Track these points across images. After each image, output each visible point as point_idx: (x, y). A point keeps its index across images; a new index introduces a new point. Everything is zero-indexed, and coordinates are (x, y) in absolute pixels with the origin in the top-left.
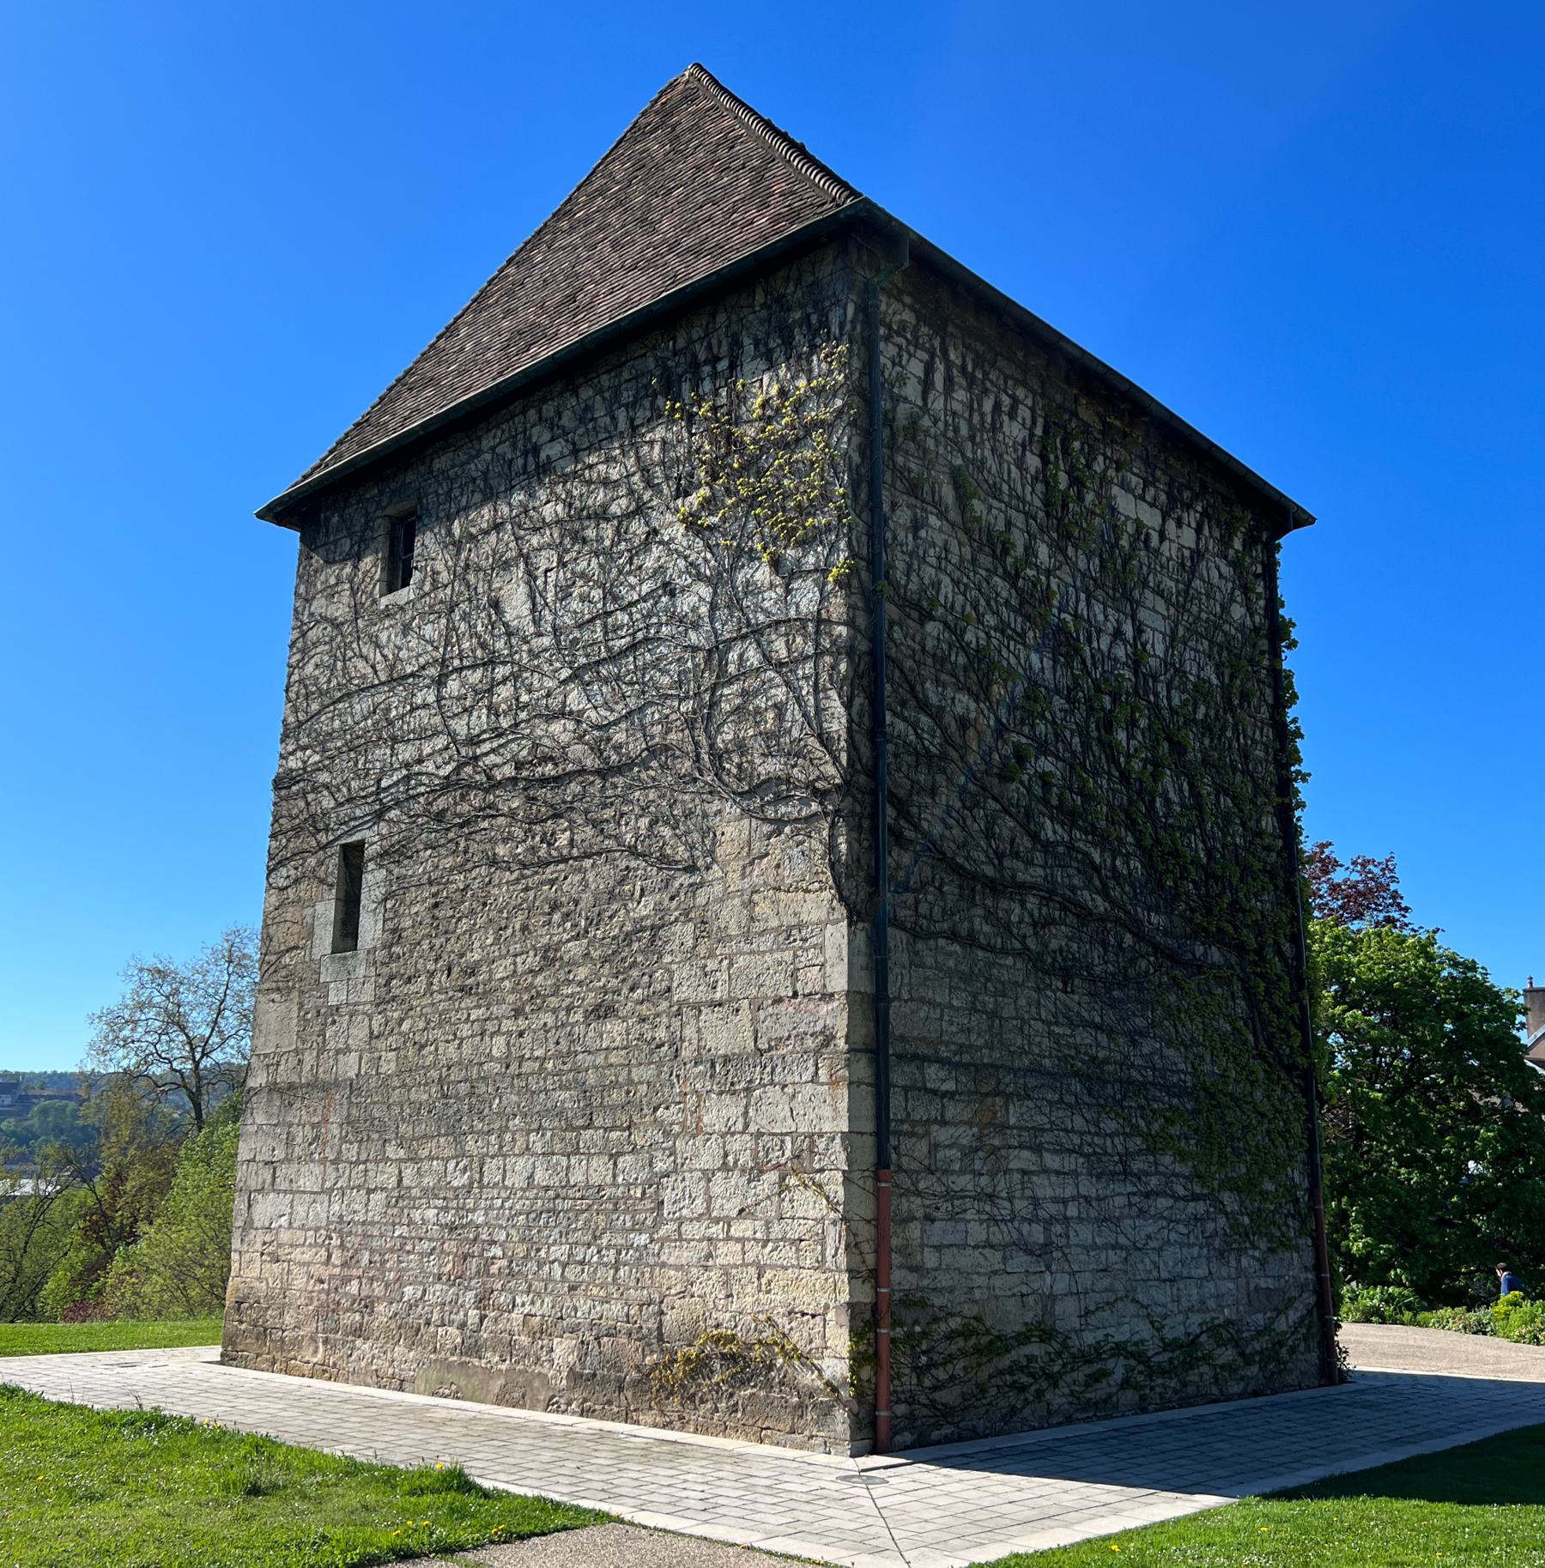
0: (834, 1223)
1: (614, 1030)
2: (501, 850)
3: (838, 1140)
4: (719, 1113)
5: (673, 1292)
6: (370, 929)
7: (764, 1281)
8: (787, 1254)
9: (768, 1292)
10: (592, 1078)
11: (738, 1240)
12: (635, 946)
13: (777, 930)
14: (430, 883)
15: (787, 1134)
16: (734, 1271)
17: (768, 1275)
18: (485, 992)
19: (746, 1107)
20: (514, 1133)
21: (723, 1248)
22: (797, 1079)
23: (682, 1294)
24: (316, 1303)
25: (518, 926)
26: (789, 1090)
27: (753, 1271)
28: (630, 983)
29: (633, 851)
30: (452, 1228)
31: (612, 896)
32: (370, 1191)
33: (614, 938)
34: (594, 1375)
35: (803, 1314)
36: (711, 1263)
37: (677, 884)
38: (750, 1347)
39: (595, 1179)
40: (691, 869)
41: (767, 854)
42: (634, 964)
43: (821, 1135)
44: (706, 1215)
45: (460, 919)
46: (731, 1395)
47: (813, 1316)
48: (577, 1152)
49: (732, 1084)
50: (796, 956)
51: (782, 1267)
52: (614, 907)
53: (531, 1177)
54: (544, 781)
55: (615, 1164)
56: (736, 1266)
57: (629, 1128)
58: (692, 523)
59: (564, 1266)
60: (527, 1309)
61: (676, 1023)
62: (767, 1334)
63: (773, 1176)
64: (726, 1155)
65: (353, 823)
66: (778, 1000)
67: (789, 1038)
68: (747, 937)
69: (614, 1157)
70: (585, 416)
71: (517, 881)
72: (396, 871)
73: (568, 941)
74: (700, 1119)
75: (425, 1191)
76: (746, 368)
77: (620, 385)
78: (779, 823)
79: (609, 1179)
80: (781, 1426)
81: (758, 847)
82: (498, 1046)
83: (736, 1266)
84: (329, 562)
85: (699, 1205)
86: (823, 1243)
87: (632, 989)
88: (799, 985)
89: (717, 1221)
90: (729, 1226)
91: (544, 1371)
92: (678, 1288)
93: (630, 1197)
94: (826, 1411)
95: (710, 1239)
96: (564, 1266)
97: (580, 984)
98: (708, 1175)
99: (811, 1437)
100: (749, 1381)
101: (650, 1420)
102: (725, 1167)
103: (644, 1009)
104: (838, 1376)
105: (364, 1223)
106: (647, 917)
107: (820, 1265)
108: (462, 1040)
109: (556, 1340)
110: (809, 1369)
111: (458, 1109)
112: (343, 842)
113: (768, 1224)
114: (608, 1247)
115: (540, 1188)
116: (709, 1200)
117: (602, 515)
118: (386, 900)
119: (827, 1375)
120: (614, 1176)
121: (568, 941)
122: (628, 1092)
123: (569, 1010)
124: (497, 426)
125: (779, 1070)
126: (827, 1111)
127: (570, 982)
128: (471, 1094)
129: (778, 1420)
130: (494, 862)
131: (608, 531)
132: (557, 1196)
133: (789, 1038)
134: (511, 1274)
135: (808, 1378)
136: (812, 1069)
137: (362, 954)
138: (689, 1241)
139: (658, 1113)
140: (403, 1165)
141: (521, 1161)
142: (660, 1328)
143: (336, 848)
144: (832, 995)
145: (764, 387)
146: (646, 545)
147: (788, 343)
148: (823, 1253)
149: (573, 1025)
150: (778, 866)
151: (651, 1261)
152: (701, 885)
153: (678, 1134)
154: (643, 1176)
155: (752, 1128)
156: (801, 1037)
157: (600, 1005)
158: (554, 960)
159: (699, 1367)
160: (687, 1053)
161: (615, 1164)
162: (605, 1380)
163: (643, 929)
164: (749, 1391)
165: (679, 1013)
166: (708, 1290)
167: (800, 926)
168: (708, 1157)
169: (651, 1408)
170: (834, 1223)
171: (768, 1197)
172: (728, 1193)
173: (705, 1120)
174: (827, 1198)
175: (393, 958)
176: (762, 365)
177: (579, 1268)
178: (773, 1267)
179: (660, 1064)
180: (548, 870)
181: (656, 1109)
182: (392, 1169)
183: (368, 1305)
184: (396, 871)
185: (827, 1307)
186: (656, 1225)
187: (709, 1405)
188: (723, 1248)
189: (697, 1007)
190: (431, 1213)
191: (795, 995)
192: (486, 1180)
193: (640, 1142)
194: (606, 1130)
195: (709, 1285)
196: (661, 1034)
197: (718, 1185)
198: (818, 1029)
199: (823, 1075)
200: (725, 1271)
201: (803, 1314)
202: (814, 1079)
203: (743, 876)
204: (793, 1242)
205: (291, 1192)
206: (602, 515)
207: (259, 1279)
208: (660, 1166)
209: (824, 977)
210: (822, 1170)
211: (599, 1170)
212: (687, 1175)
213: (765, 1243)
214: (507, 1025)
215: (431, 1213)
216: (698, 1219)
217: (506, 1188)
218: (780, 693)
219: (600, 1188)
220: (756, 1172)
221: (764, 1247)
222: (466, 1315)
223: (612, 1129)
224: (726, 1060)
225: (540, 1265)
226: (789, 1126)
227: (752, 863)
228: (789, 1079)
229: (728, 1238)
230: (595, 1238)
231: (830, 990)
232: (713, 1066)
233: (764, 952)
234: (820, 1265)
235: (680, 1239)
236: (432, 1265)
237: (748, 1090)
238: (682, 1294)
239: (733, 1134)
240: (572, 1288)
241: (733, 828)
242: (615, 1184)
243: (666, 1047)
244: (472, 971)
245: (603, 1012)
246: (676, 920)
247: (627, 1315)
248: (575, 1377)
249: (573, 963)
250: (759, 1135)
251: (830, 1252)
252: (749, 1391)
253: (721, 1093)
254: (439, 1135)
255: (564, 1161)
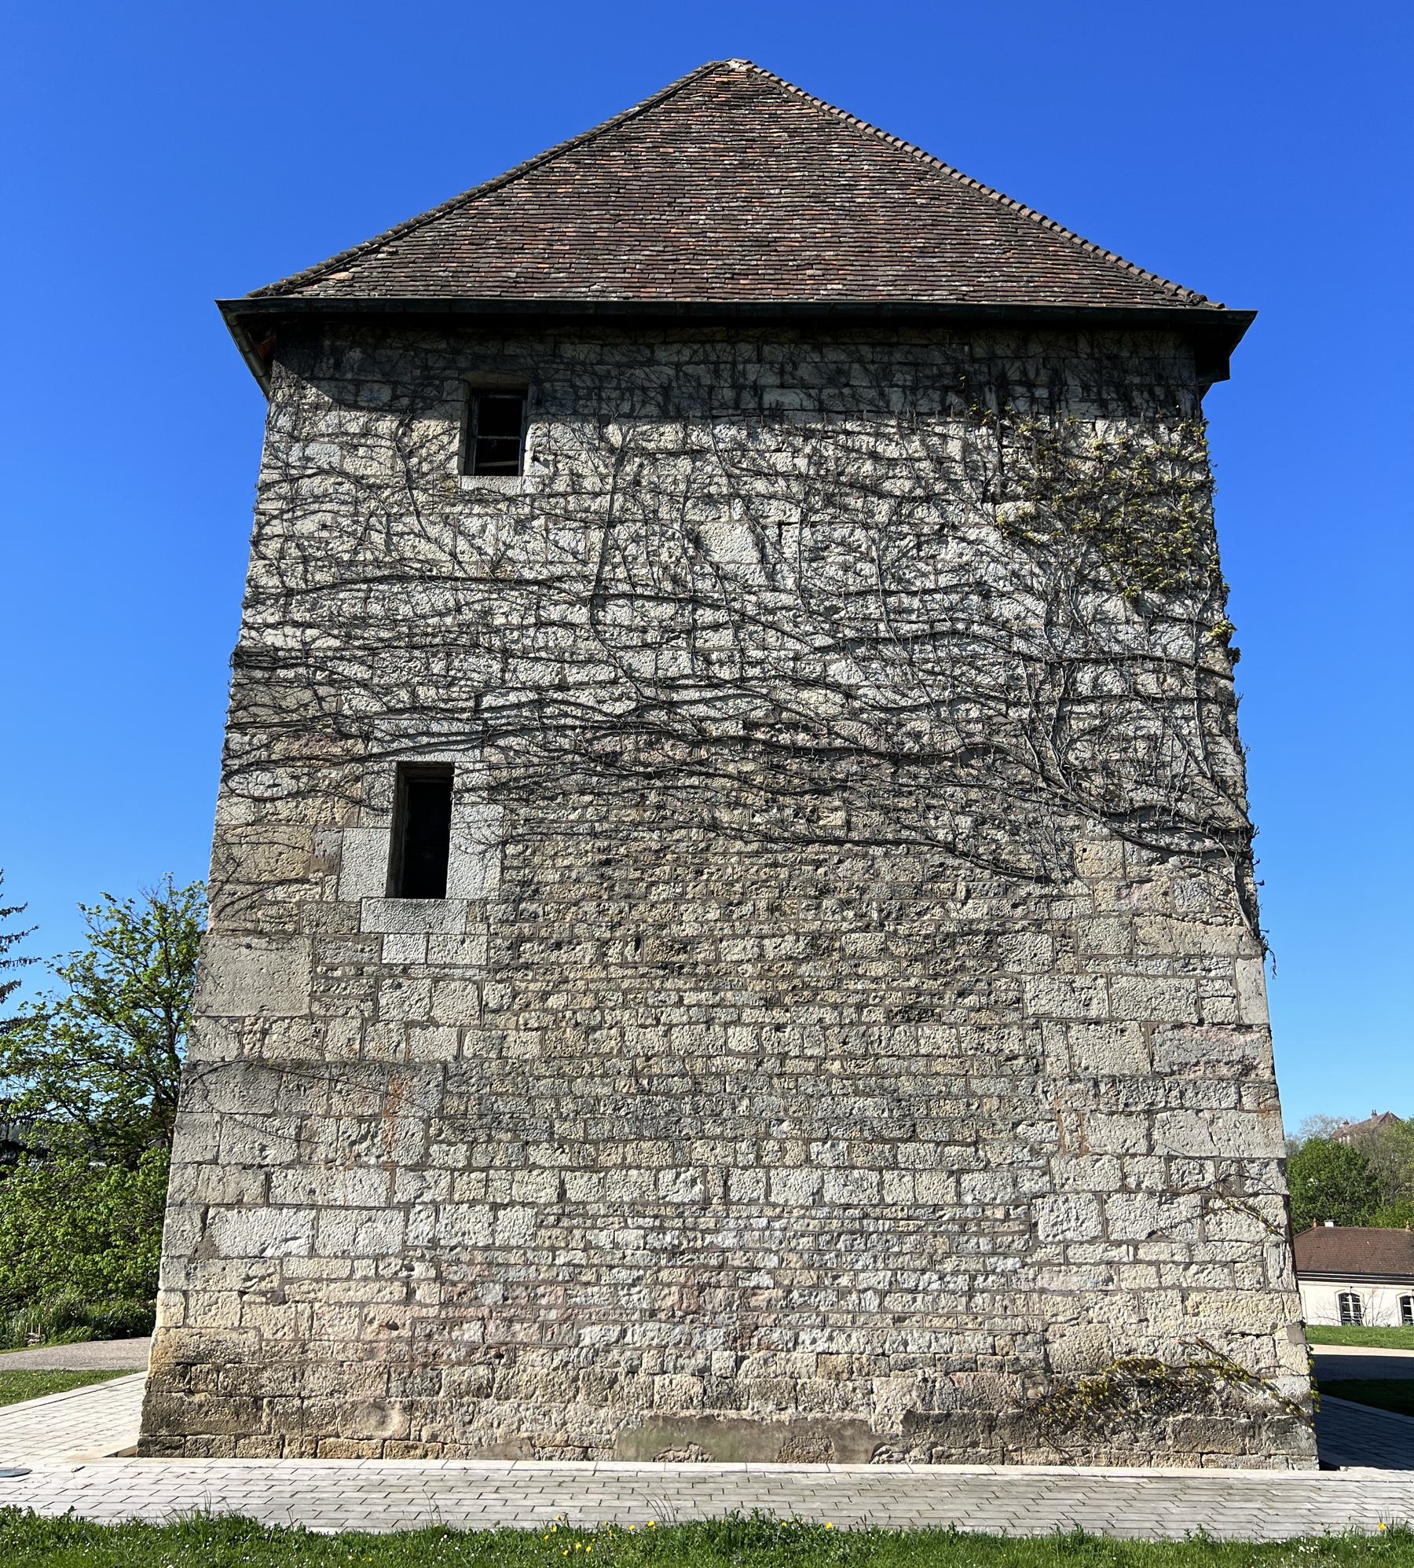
0: (1277, 1245)
1: (935, 1036)
2: (724, 816)
3: (1274, 1165)
4: (1110, 1133)
5: (1060, 1318)
6: (469, 872)
7: (1189, 1303)
8: (1220, 1277)
9: (1196, 1315)
10: (907, 1086)
11: (1150, 1263)
12: (962, 950)
13: (1173, 957)
14: (594, 835)
15: (1207, 1158)
16: (1147, 1295)
17: (1194, 1297)
18: (708, 975)
19: (1149, 1129)
20: (782, 1142)
21: (1127, 1272)
22: (1215, 1105)
23: (1074, 1321)
24: (382, 1356)
25: (762, 905)
26: (1207, 1115)
27: (1175, 1295)
28: (957, 986)
29: (950, 848)
30: (674, 1252)
31: (919, 892)
32: (495, 1207)
33: (927, 937)
34: (948, 1415)
35: (1243, 1335)
36: (1111, 1287)
37: (1023, 893)
38: (1177, 1371)
39: (927, 1197)
40: (1044, 880)
41: (1150, 880)
42: (962, 968)
43: (1252, 1161)
44: (1104, 1237)
45: (653, 884)
46: (1156, 1422)
47: (1258, 1336)
48: (894, 1166)
49: (1126, 1105)
50: (1198, 985)
51: (1214, 1289)
52: (925, 903)
53: (819, 1192)
54: (798, 751)
55: (958, 1182)
56: (1151, 1290)
57: (975, 1143)
58: (1012, 532)
59: (883, 1295)
60: (821, 1346)
61: (1033, 1037)
62: (1201, 1356)
63: (1195, 1199)
64: (1125, 1177)
65: (425, 740)
66: (1180, 1026)
67: (1197, 1064)
68: (1130, 957)
69: (957, 1174)
70: (837, 377)
71: (757, 854)
72: (523, 812)
73: (852, 931)
74: (1083, 1138)
75: (615, 1208)
76: (1073, 406)
77: (891, 364)
78: (1165, 853)
79: (950, 1198)
80: (1229, 1449)
81: (1134, 871)
82: (740, 1039)
83: (1151, 1290)
84: (341, 403)
85: (1092, 1228)
86: (1263, 1263)
87: (961, 994)
88: (1205, 1013)
89: (1119, 1244)
90: (1136, 1249)
91: (861, 1416)
92: (1069, 1315)
93: (987, 1219)
94: (1283, 1430)
95: (1109, 1263)
96: (883, 1295)
97: (876, 980)
98: (1101, 1198)
99: (1270, 1456)
100: (1180, 1405)
101: (1042, 1459)
102: (1124, 1189)
103: (984, 1017)
104: (1298, 1393)
105: (487, 1248)
106: (979, 921)
107: (1263, 1286)
108: (671, 1026)
109: (876, 1382)
110: (1260, 1388)
111: (670, 1109)
112: (404, 758)
113: (1190, 1247)
114: (955, 1273)
115: (833, 1205)
116: (1105, 1223)
117: (871, 489)
118: (504, 843)
119: (1284, 1393)
120: (959, 1194)
121: (852, 931)
122: (969, 1105)
123: (859, 1007)
124: (685, 343)
125: (1190, 1094)
126: (1257, 1137)
127: (859, 977)
128: (696, 1092)
129: (1224, 1443)
130: (714, 826)
131: (883, 510)
132: (866, 1216)
133: (1197, 1064)
134: (790, 1307)
135: (1259, 1398)
136: (1235, 1097)
137: (455, 907)
138: (1080, 1265)
139: (1020, 1129)
140: (568, 1176)
141: (797, 1177)
142: (1046, 1356)
143: (389, 764)
144: (1250, 1027)
145: (1102, 433)
146: (940, 537)
147: (1171, 400)
148: (1264, 1274)
149: (869, 1025)
150: (1165, 894)
151: (1024, 1287)
152: (1059, 897)
153: (1053, 1154)
154: (1008, 1194)
155: (1158, 1151)
156: (1212, 1064)
157: (911, 1007)
158: (829, 951)
159: (1107, 1397)
160: (1052, 1068)
161: (958, 1182)
162: (966, 1421)
163: (977, 933)
164: (1180, 1417)
165: (1037, 1026)
166: (1112, 1315)
167: (1202, 956)
168: (1102, 1176)
169: (1039, 1446)
170: (1277, 1245)
171: (1189, 1220)
172: (1132, 1217)
173: (1092, 1139)
174: (1265, 1221)
175: (519, 916)
176: (1094, 409)
177: (910, 1297)
178: (1198, 1290)
179: (1014, 1078)
180: (810, 849)
181: (1015, 1125)
182: (550, 1179)
183: (506, 1353)
184: (523, 811)
185: (1274, 1326)
186: (1029, 1250)
187: (1125, 1435)
188: (1127, 1272)
189: (1065, 1023)
190: (632, 1236)
191: (1201, 1022)
192: (734, 1195)
193: (995, 1160)
194: (938, 1144)
195: (1116, 1311)
196: (1012, 1045)
197: (1116, 1206)
198: (1235, 1057)
199: (1248, 1102)
200: (1135, 1294)
201: (1243, 1335)
202: (1238, 1106)
203: (1119, 897)
204: (1225, 1264)
205: (312, 1207)
206: (871, 489)
207: (241, 1329)
208: (1027, 1186)
209: (1238, 1008)
210: (1256, 1194)
211: (933, 1188)
212: (1072, 1197)
213: (1187, 1266)
214: (760, 1015)
215: (632, 1236)
216: (1092, 1241)
217: (775, 1206)
218: (1154, 727)
219: (936, 1207)
220: (1171, 1194)
221: (1186, 1269)
222: (709, 1358)
223: (948, 1143)
224: (1114, 1080)
225: (842, 1294)
226: (1209, 1149)
227: (1129, 886)
228: (1204, 1104)
229: (1137, 1262)
230: (932, 1261)
231: (1247, 1022)
232: (1096, 1085)
233: (1155, 977)
234: (1263, 1286)
235: (1067, 1263)
236: (640, 1298)
237: (1150, 1113)
238: (1074, 1321)
239: (1134, 1156)
240: (899, 1320)
241: (1098, 851)
242: (959, 1204)
243: (1021, 1061)
244: (686, 945)
245: (915, 1013)
246: (1024, 929)
247: (993, 1347)
248: (911, 1418)
249: (859, 958)
250: (1170, 1159)
251: (1272, 1273)
252: (1180, 1417)
253: (1112, 1114)
254: (641, 1138)
255: (874, 1177)
